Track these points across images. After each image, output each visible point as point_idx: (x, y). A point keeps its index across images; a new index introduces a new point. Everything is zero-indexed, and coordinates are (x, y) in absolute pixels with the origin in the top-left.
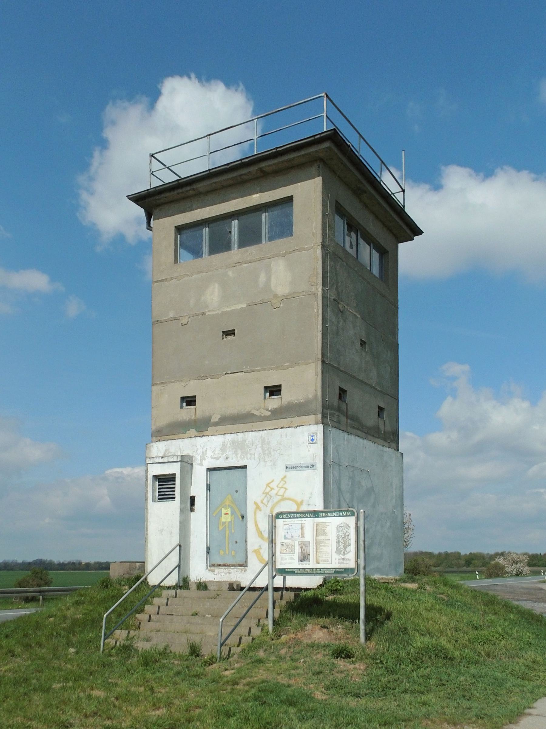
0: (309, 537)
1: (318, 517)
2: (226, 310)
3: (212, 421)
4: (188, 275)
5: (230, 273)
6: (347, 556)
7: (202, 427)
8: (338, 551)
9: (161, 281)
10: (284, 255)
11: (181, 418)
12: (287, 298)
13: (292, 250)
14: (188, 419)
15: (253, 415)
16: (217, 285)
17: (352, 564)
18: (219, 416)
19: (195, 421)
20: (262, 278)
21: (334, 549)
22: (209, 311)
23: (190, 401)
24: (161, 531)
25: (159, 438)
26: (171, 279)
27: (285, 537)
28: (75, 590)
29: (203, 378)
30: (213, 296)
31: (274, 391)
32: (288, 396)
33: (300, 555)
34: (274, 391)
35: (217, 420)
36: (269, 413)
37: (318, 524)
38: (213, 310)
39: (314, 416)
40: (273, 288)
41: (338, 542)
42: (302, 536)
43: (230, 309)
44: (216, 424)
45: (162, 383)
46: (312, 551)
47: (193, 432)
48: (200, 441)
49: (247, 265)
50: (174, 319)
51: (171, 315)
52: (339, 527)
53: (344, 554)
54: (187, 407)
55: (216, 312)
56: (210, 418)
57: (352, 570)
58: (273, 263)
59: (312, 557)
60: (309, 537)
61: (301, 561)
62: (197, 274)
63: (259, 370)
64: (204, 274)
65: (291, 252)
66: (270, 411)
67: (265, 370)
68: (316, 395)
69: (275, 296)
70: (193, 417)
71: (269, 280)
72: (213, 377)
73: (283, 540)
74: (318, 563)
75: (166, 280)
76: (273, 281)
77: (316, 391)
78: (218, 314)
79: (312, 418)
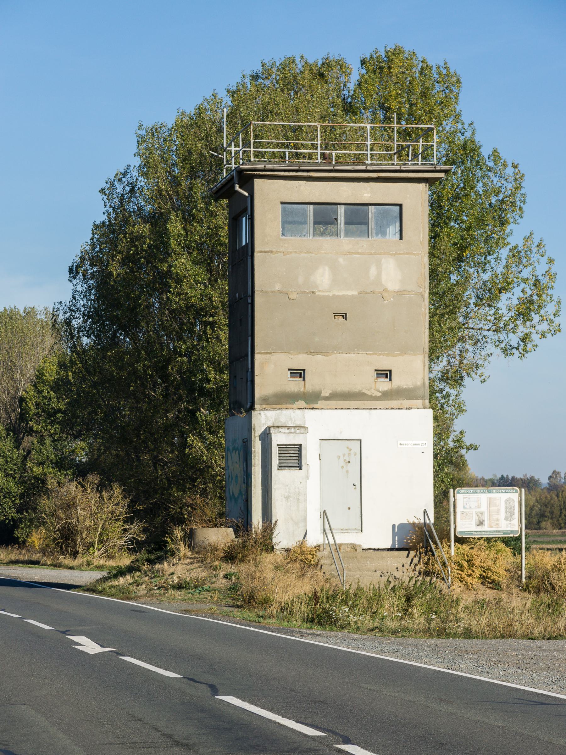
0: (484, 508)
1: (491, 493)
2: (337, 293)
3: (323, 395)
4: (296, 253)
5: (341, 260)
6: (512, 522)
7: (312, 399)
8: (506, 519)
9: (265, 252)
10: (393, 255)
11: (289, 389)
12: (399, 293)
13: (402, 252)
14: (296, 391)
15: (364, 394)
16: (327, 268)
17: (516, 528)
18: (330, 392)
19: (304, 393)
20: (373, 271)
21: (503, 517)
22: (319, 291)
23: (299, 373)
24: (287, 498)
25: (264, 406)
26: (277, 252)
27: (464, 508)
28: (482, 538)
29: (313, 354)
30: (323, 280)
31: (386, 374)
32: (398, 381)
33: (477, 521)
34: (386, 374)
35: (327, 395)
36: (379, 394)
37: (490, 498)
38: (322, 291)
39: (421, 401)
40: (383, 283)
41: (506, 512)
42: (479, 507)
43: (341, 294)
44: (326, 399)
45: (267, 353)
46: (486, 518)
47: (301, 403)
48: (309, 413)
49: (358, 256)
50: (281, 292)
51: (278, 287)
52: (507, 500)
53: (511, 520)
54: (292, 379)
55: (327, 294)
56: (320, 393)
57: (517, 532)
58: (383, 260)
59: (486, 523)
60: (484, 508)
61: (478, 526)
62: (306, 253)
63: (370, 354)
64: (314, 255)
65: (400, 254)
66: (380, 392)
67: (376, 354)
68: (424, 383)
69: (386, 290)
70: (302, 389)
71: (379, 274)
72: (321, 353)
73: (463, 510)
74: (491, 527)
75: (271, 252)
76: (384, 277)
77: (424, 379)
78: (328, 296)
79: (419, 402)
